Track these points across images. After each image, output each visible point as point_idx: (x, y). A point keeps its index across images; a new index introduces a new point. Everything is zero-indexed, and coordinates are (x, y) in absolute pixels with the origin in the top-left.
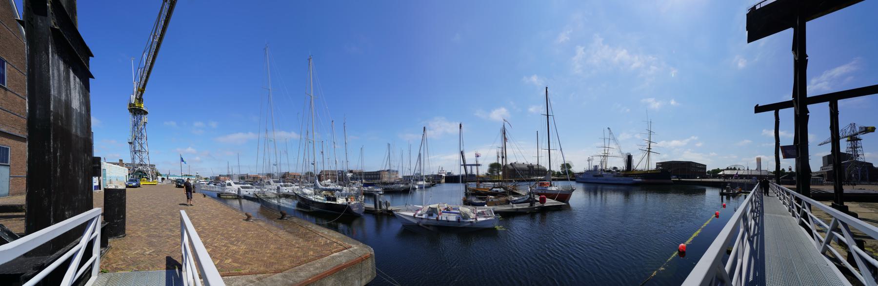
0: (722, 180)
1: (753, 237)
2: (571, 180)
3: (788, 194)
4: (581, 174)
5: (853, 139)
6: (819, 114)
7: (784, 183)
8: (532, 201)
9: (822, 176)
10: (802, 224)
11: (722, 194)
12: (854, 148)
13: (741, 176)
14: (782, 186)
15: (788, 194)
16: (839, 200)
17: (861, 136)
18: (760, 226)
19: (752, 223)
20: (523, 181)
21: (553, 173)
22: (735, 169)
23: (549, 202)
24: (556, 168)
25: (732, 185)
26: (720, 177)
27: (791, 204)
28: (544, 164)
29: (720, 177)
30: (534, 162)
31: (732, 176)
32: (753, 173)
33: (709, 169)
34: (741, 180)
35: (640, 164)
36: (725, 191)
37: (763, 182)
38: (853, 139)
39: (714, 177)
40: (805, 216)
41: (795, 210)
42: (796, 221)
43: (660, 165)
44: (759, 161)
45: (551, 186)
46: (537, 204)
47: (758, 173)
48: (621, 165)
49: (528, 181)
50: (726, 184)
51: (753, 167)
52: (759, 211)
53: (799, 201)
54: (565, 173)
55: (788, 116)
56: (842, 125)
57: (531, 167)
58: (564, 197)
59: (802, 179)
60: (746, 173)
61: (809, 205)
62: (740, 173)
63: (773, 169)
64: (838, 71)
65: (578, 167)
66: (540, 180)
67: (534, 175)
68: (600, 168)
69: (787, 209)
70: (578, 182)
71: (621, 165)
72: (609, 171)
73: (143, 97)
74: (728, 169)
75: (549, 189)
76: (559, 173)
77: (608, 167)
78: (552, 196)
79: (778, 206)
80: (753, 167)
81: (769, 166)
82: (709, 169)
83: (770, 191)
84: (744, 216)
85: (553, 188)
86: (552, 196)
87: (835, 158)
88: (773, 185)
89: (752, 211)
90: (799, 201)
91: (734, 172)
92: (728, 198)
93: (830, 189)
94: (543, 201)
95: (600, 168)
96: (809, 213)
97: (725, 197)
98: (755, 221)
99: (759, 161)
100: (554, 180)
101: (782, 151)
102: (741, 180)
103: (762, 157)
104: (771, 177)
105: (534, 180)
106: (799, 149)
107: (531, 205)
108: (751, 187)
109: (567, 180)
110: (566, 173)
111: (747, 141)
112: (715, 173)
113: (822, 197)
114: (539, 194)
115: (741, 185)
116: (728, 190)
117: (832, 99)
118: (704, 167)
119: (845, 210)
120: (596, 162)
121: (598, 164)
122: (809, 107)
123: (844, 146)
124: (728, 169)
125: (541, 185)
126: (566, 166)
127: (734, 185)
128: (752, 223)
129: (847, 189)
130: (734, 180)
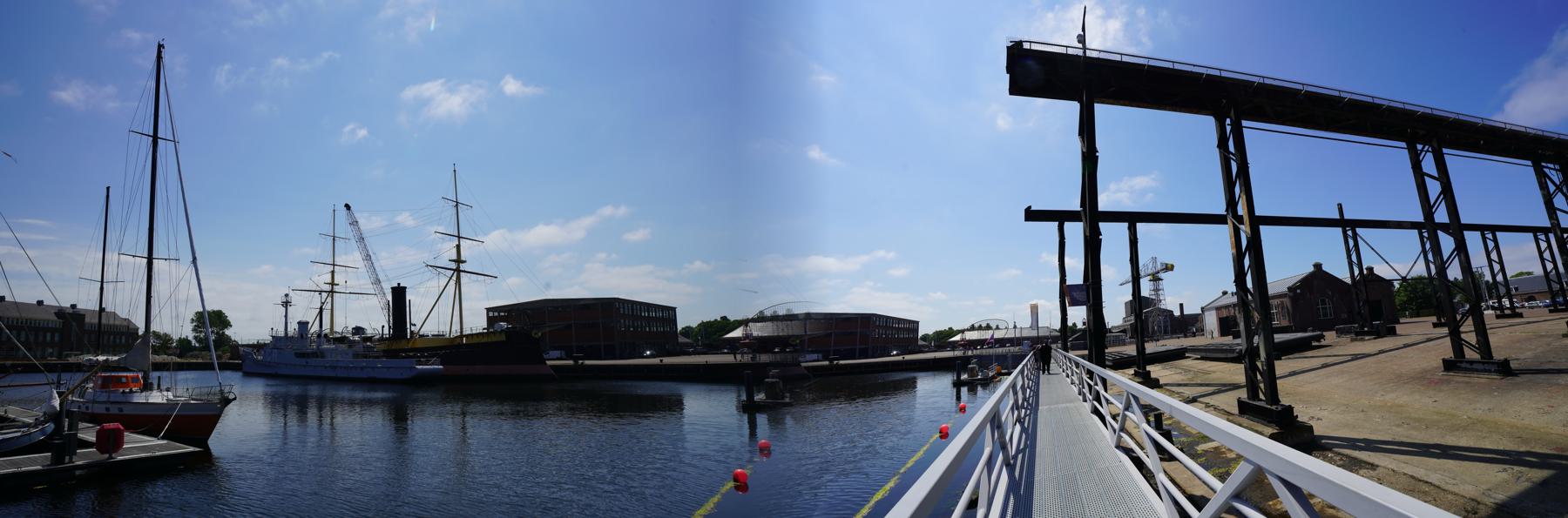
0: (958, 353)
1: (1015, 457)
2: (224, 367)
3: (1077, 365)
4: (259, 347)
5: (1156, 279)
6: (1113, 236)
7: (1074, 348)
8: (60, 443)
9: (1124, 331)
10: (1096, 412)
11: (958, 385)
12: (1157, 290)
13: (1002, 342)
14: (1071, 354)
15: (1077, 365)
16: (1140, 365)
17: (1161, 275)
18: (1030, 434)
19: (1014, 433)
20: (31, 369)
21: (164, 342)
22: (988, 327)
23: (137, 445)
24: (175, 323)
25: (972, 361)
26: (954, 346)
27: (1081, 381)
28: (126, 305)
29: (954, 346)
30: (86, 301)
31: (981, 342)
32: (1026, 334)
33: (925, 329)
34: (1000, 350)
35: (432, 317)
36: (964, 377)
37: (1041, 350)
38: (1156, 279)
39: (940, 348)
40: (1098, 398)
41: (1086, 390)
42: (1087, 406)
43: (495, 315)
44: (1034, 310)
45: (147, 387)
46: (83, 457)
47: (1034, 334)
48: (376, 322)
49: (51, 368)
50: (967, 360)
51: (1025, 322)
52: (1029, 407)
53: (1090, 374)
54: (204, 342)
55: (1075, 231)
56: (1143, 259)
57: (70, 318)
58: (196, 424)
59: (1094, 340)
60: (1011, 335)
61: (1104, 381)
62: (999, 335)
63: (1057, 324)
64: (1141, 182)
65: (252, 326)
66: (106, 366)
67: (83, 350)
68: (315, 328)
69: (1076, 390)
70: (248, 374)
71: (376, 322)
72: (342, 340)
73: (967, 326)
74: (972, 328)
75: (140, 398)
76: (184, 342)
77: (338, 328)
78: (149, 422)
79: (1062, 388)
80: (1025, 322)
81: (1050, 320)
82: (925, 329)
83: (1053, 365)
84: (994, 420)
85: (156, 397)
86: (149, 422)
87: (1138, 304)
88: (1057, 353)
89: (1016, 406)
90: (1090, 374)
91: (987, 335)
92: (972, 390)
93: (1131, 350)
94: (110, 441)
95: (315, 328)
96: (1102, 392)
97: (964, 390)
98: (1022, 424)
99: (1034, 310)
100: (158, 367)
101: (1068, 295)
102: (1000, 350)
103: (1041, 303)
104: (1055, 339)
105: (78, 368)
106: (1090, 292)
107: (58, 459)
108: (1018, 359)
109: (208, 367)
110: (211, 345)
111: (1014, 272)
112: (942, 339)
113: (1120, 364)
114: (93, 419)
115: (1001, 359)
116: (972, 372)
117: (1132, 219)
118: (913, 326)
119: (1154, 384)
120: (304, 310)
121: (311, 317)
122: (1102, 225)
123: (1146, 289)
124: (972, 328)
125: (106, 384)
126: (214, 321)
127: (984, 362)
128: (1014, 433)
129: (1151, 348)
130: (986, 351)
